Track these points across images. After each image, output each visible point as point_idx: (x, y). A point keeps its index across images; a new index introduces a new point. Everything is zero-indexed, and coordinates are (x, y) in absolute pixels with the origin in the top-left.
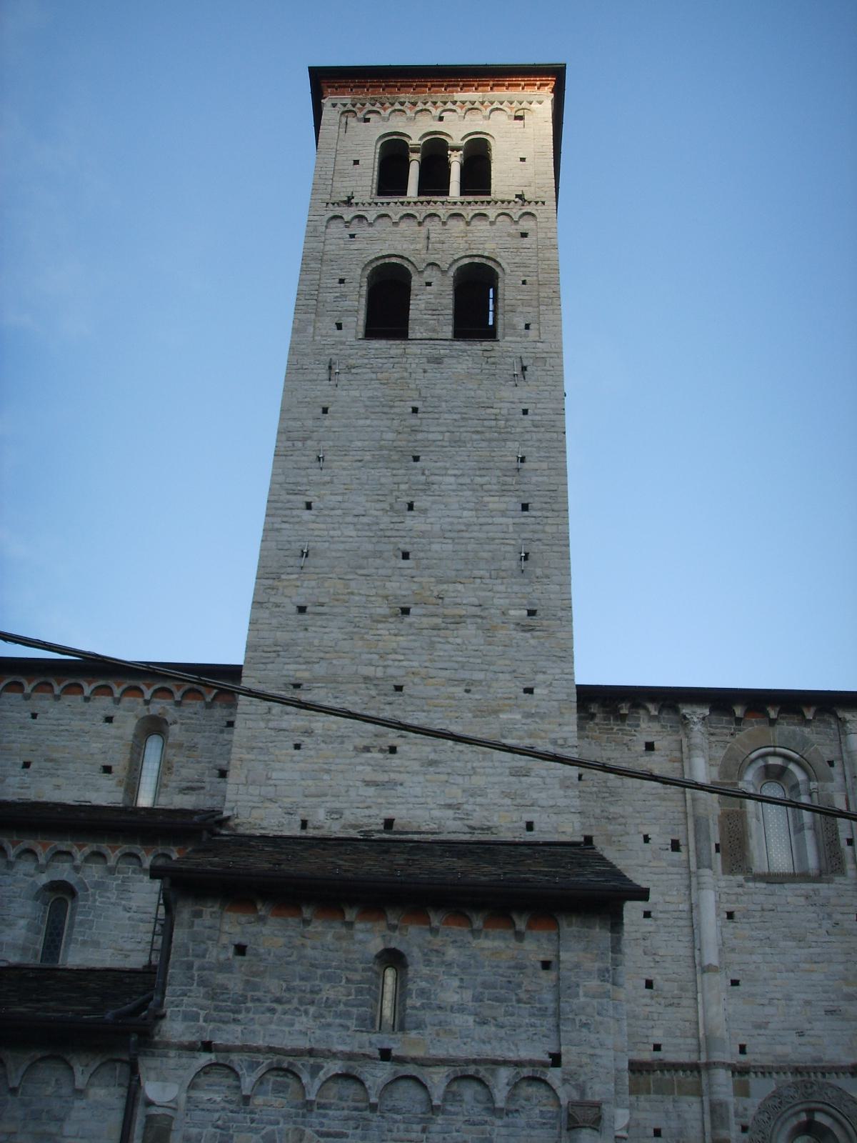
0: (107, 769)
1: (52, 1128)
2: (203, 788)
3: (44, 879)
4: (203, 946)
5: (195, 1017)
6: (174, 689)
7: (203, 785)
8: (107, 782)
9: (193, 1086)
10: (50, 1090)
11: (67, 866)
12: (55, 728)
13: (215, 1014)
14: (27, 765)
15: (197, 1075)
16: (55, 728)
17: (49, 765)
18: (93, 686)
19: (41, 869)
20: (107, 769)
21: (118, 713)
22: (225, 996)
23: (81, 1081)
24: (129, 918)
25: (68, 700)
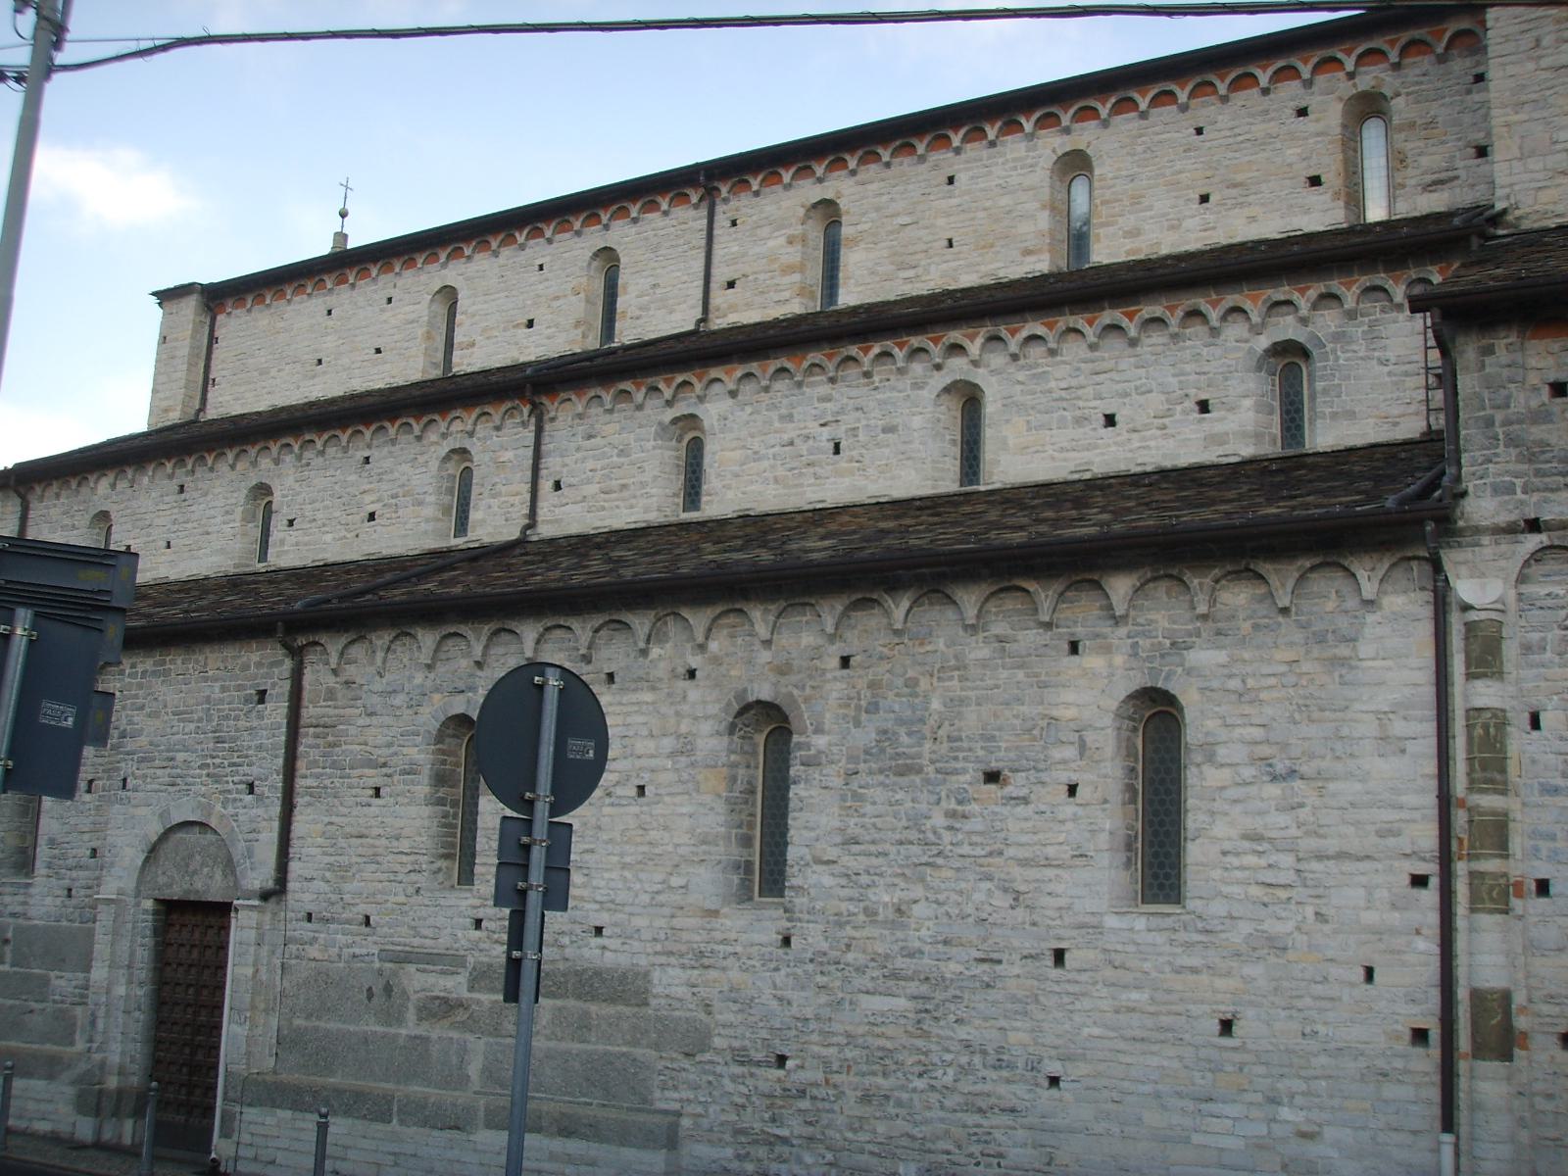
0: (1315, 181)
1: (1343, 651)
2: (1456, 178)
3: (1263, 342)
4: (1503, 392)
5: (1510, 490)
6: (1385, 47)
7: (1455, 173)
8: (1317, 198)
9: (1522, 579)
10: (1330, 605)
11: (1290, 319)
12: (1231, 140)
13: (1536, 481)
14: (1204, 199)
15: (1526, 564)
16: (1231, 140)
17: (1234, 192)
18: (1270, 71)
19: (1257, 330)
20: (1315, 181)
21: (1313, 101)
22: (1548, 456)
23: (1369, 589)
24: (1390, 374)
25: (1240, 98)
